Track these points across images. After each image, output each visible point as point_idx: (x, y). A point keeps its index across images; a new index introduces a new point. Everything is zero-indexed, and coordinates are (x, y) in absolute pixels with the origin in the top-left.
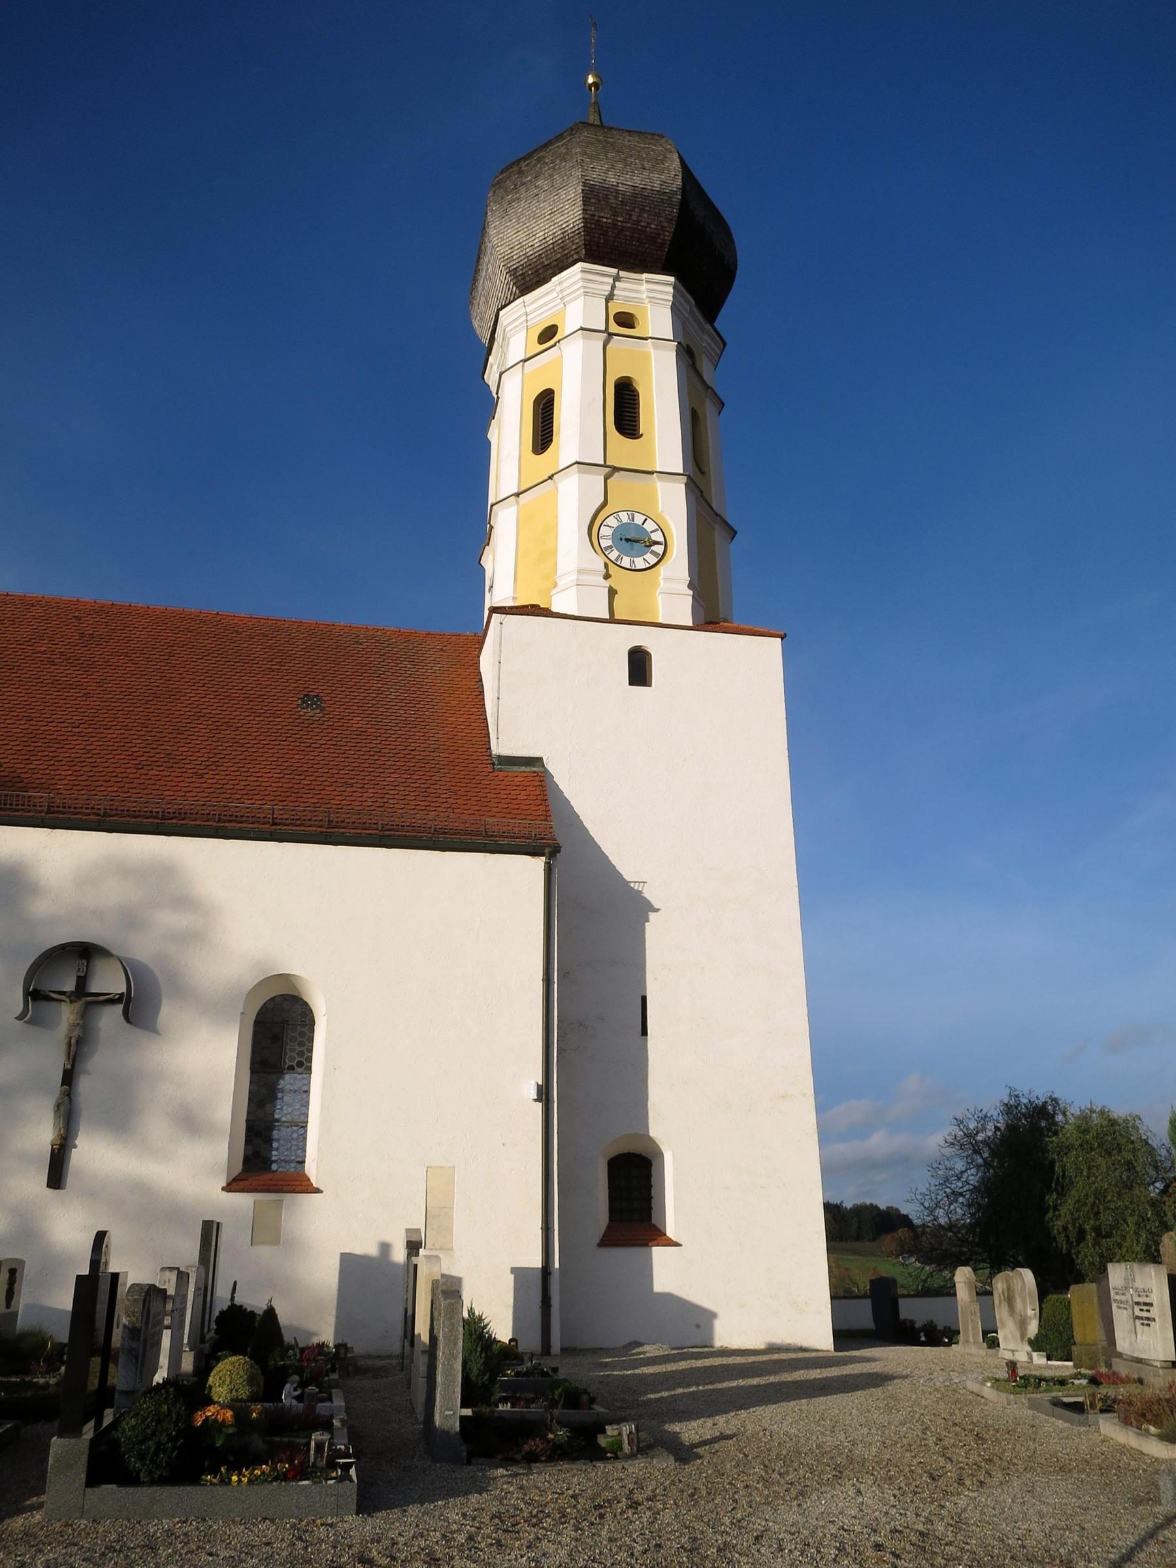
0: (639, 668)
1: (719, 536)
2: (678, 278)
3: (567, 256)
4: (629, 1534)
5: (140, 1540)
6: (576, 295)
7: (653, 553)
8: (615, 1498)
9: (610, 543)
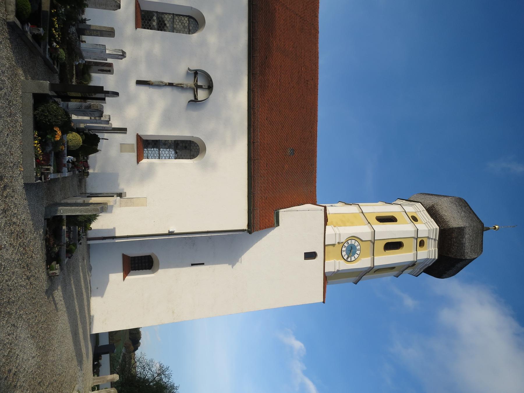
0: (310, 256)
1: (355, 279)
2: (437, 260)
3: (440, 223)
4: (16, 278)
5: (14, 111)
6: (428, 227)
7: (348, 258)
8: (31, 271)
9: (350, 243)
